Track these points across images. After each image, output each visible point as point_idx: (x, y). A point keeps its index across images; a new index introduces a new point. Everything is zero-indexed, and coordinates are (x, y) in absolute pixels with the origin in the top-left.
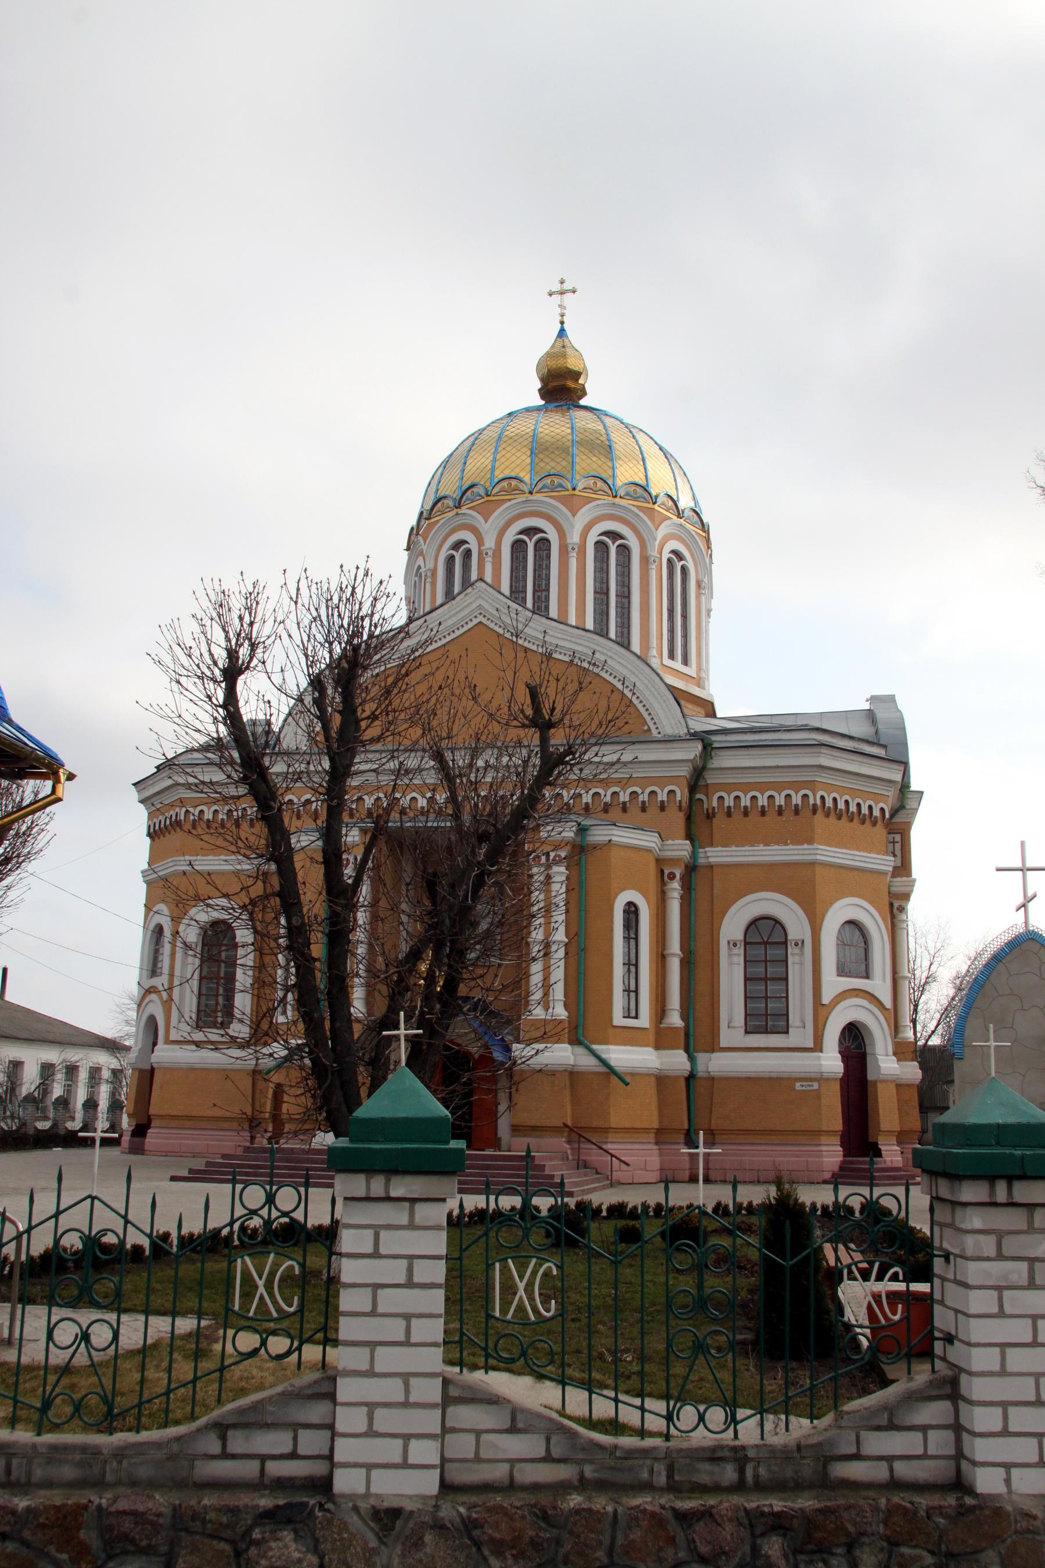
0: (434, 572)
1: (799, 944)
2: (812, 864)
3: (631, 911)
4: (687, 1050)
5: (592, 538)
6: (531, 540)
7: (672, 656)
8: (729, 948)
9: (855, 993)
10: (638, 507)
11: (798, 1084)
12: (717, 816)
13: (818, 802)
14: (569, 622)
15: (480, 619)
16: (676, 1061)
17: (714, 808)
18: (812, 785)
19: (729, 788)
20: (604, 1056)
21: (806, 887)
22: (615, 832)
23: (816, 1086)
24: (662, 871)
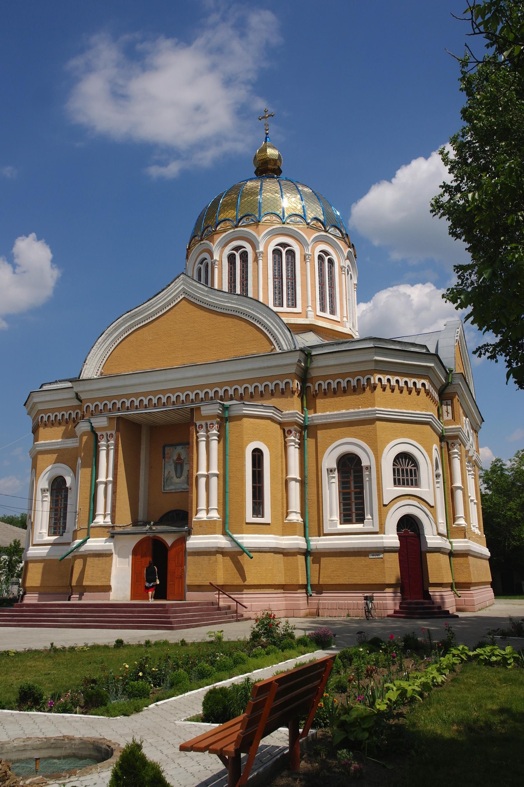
1: (368, 468)
3: (257, 455)
4: (305, 536)
7: (323, 309)
8: (328, 474)
9: (408, 497)
14: (223, 290)
17: (316, 391)
19: (325, 378)
20: (239, 541)
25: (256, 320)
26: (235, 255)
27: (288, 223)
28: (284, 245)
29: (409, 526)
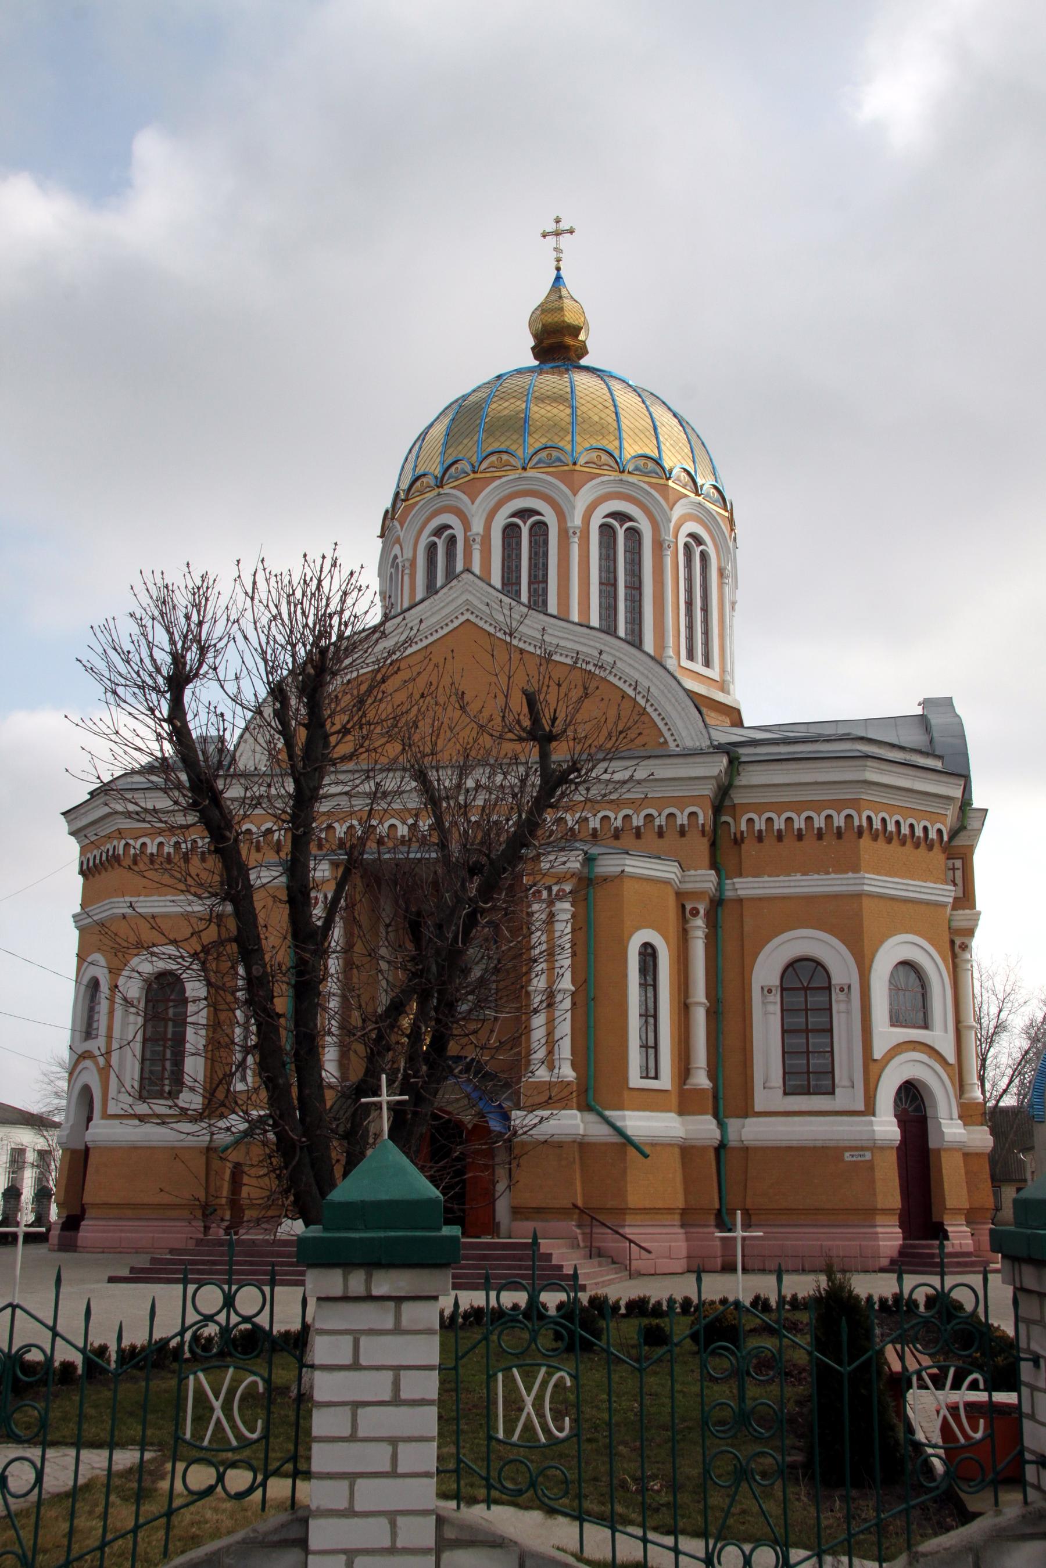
0: (413, 562)
2: (859, 896)
3: (648, 953)
4: (716, 1116)
5: (597, 520)
6: (525, 523)
7: (691, 656)
9: (911, 1046)
10: (649, 484)
11: (847, 1154)
12: (746, 841)
13: (865, 823)
15: (467, 616)
16: (703, 1128)
17: (742, 832)
18: (855, 803)
20: (619, 1124)
21: (849, 921)
22: (628, 862)
23: (868, 1156)
24: (683, 907)
25: (625, 682)
26: (520, 528)
27: (629, 472)
28: (621, 517)
29: (912, 1100)
